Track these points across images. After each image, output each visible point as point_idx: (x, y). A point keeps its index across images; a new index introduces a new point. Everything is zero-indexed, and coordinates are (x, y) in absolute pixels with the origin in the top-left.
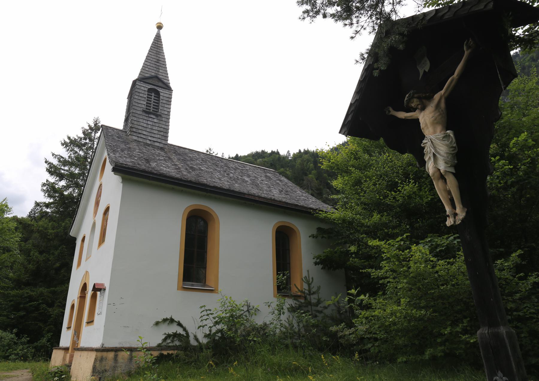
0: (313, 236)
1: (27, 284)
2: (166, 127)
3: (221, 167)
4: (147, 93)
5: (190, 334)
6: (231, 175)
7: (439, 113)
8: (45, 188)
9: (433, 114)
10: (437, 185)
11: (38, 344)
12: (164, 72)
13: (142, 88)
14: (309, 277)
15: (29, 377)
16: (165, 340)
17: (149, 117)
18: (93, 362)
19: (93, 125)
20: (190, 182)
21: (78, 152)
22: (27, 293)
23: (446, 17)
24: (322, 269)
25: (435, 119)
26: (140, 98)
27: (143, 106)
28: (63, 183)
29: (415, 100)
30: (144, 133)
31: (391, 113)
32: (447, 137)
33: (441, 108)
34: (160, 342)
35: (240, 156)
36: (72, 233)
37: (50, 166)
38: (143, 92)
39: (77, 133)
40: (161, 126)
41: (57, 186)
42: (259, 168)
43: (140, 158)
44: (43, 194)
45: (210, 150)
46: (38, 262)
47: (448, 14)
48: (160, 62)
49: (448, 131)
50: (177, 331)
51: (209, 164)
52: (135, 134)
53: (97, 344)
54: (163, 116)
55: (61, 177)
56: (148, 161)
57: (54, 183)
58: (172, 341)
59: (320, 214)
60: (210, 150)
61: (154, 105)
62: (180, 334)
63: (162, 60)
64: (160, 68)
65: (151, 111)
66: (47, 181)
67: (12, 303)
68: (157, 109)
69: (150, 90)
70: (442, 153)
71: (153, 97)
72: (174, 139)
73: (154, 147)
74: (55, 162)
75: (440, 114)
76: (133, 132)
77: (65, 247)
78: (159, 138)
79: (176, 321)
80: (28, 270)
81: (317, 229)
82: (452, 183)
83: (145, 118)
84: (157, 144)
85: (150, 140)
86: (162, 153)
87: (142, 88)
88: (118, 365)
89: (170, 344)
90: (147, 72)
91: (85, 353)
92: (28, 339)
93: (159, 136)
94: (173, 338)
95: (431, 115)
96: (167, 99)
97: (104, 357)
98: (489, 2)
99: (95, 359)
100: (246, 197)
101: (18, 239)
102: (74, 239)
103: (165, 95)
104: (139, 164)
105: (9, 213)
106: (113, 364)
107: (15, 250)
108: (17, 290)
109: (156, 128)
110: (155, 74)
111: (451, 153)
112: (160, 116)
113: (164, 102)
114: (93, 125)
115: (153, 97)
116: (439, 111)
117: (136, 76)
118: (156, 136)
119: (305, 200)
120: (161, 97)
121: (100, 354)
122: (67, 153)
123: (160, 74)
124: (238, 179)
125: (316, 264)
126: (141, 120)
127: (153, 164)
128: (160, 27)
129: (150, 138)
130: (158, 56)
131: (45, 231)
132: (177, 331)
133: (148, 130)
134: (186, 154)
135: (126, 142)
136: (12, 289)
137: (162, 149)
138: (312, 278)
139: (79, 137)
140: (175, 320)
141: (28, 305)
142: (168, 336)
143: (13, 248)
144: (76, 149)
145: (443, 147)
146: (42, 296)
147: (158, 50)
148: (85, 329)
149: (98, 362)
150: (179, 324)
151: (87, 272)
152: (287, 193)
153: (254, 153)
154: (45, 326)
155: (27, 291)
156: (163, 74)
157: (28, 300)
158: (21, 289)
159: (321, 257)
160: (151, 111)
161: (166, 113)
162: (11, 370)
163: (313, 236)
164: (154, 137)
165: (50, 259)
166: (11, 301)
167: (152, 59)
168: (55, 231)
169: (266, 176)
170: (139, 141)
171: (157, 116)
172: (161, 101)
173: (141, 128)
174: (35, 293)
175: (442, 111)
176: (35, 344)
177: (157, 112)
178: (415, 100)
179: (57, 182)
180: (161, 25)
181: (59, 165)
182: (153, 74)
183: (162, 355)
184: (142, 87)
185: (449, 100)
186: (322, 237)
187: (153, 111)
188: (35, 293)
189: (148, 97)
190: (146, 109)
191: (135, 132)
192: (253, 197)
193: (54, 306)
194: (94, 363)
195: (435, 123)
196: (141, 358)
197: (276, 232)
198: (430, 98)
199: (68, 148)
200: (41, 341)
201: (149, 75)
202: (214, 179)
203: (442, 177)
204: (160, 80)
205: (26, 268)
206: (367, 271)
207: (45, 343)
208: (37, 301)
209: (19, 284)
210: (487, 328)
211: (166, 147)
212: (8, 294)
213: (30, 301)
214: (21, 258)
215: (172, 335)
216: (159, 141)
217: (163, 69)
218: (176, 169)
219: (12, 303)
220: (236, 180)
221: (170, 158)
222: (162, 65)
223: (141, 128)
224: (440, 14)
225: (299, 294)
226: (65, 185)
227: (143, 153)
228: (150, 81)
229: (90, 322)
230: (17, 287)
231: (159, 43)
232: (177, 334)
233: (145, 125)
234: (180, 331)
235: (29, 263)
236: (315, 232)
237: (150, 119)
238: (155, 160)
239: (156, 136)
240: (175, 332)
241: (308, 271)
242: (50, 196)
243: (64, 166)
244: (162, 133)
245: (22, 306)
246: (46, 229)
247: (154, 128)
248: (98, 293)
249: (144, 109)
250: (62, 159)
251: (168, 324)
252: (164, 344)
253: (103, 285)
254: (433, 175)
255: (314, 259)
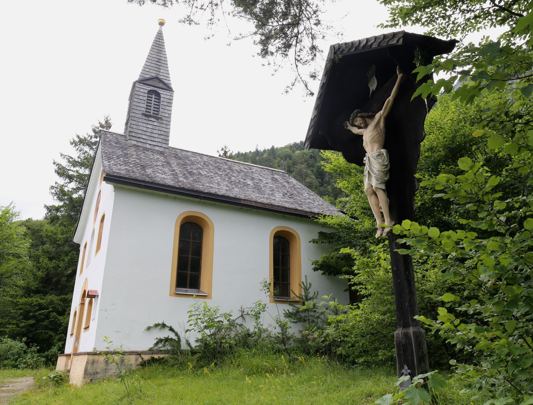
0: (314, 241)
1: (37, 292)
2: (166, 130)
3: (224, 171)
4: (146, 95)
5: (181, 339)
6: (233, 178)
7: (376, 132)
8: (53, 191)
9: (372, 132)
10: (371, 201)
11: (49, 353)
12: (166, 72)
13: (142, 90)
14: (306, 282)
15: (32, 382)
16: (157, 344)
17: (149, 120)
18: (85, 365)
19: (103, 123)
20: (183, 189)
21: (88, 151)
22: (36, 301)
23: (373, 46)
24: (322, 274)
25: (373, 138)
26: (139, 101)
27: (143, 109)
28: (73, 185)
29: (358, 119)
30: (144, 137)
31: (348, 128)
32: (380, 155)
33: (379, 127)
34: (152, 346)
35: (277, 148)
36: (76, 240)
37: (58, 167)
38: (142, 94)
39: (86, 132)
40: (161, 129)
41: (66, 189)
42: (267, 169)
43: (135, 165)
44: (51, 196)
45: (226, 147)
46: (48, 269)
47: (375, 44)
48: (162, 61)
49: (382, 150)
50: (168, 336)
51: (211, 167)
52: (134, 139)
53: (90, 350)
54: (163, 118)
55: (71, 178)
56: (143, 167)
57: (63, 185)
58: (164, 346)
59: (320, 219)
60: (226, 147)
61: (154, 107)
62: (172, 339)
63: (163, 59)
64: (161, 68)
65: (151, 113)
66: (56, 183)
67: (21, 311)
68: (157, 111)
69: (150, 92)
70: (375, 170)
71: (153, 99)
72: (172, 143)
73: (153, 151)
74: (64, 163)
75: (378, 133)
76: (133, 136)
77: (75, 253)
78: (159, 142)
79: (168, 327)
80: (38, 277)
81: (319, 233)
82: (382, 196)
83: (145, 122)
84: (157, 148)
85: (150, 144)
86: (162, 158)
87: (142, 90)
88: (109, 368)
89: (162, 349)
90: (147, 73)
91: (80, 357)
92: (38, 348)
93: (159, 140)
94: (165, 343)
95: (370, 134)
96: (168, 101)
97: (95, 360)
98: (400, 38)
99: (87, 362)
100: (242, 202)
101: (28, 245)
102: (78, 246)
103: (166, 97)
104: (133, 172)
105: (17, 217)
106: (105, 367)
107: (25, 256)
108: (26, 298)
109: (157, 132)
110: (156, 75)
111: (382, 171)
112: (161, 118)
113: (165, 104)
114: (103, 123)
115: (153, 99)
116: (377, 131)
117: (137, 78)
118: (156, 140)
119: (310, 203)
120: (162, 99)
121: (91, 357)
122: (76, 152)
123: (161, 74)
124: (239, 182)
125: (315, 269)
126: (141, 124)
127: (149, 171)
128: (162, 24)
129: (150, 142)
130: (160, 55)
131: (55, 237)
132: (168, 336)
133: (148, 134)
134: (187, 158)
135: (123, 148)
136: (22, 296)
137: (162, 153)
138: (310, 284)
139: (90, 136)
140: (167, 325)
141: (37, 313)
142: (160, 341)
143: (23, 254)
144: (86, 148)
145: (376, 165)
146: (52, 304)
147: (160, 49)
148: (83, 334)
149: (90, 365)
150: (171, 329)
151: (86, 279)
152: (291, 196)
153: (291, 144)
154: (56, 335)
155: (36, 299)
156: (165, 75)
157: (37, 308)
158: (30, 297)
159: (318, 262)
160: (151, 113)
161: (167, 115)
162: (18, 377)
163: (314, 241)
164: (154, 141)
165: (60, 265)
166: (21, 309)
167: (152, 59)
168: (64, 236)
169: (273, 179)
170: (138, 146)
171: (157, 119)
172: (162, 103)
173: (140, 132)
174: (45, 301)
175: (380, 130)
176: (46, 353)
177: (157, 114)
178: (358, 119)
179: (66, 185)
180: (163, 21)
181: (69, 166)
182: (154, 75)
183: (153, 359)
184: (142, 89)
185: (389, 120)
186: (322, 242)
187: (153, 113)
188: (45, 301)
189: (147, 99)
190: (146, 111)
191: (134, 136)
192: (249, 202)
193: (65, 314)
194: (86, 365)
195: (373, 141)
196: (132, 360)
197: (274, 237)
198: (372, 117)
199: (77, 147)
200: (51, 350)
201: (149, 76)
202: (213, 184)
203: (375, 193)
204: (160, 81)
205: (36, 275)
206: (344, 277)
207: (55, 352)
208: (47, 309)
209: (28, 292)
210: (402, 328)
211: (167, 150)
212: (17, 302)
213: (40, 310)
214: (30, 264)
215: (163, 340)
216: (159, 144)
217: (164, 68)
218: (173, 175)
219: (21, 311)
220: (236, 184)
221: (168, 163)
222: (163, 65)
223: (140, 132)
224: (370, 43)
225: (298, 299)
226: (75, 187)
227: (140, 159)
228: (150, 82)
229: (87, 328)
230: (26, 295)
231: (161, 41)
232: (169, 339)
233: (145, 129)
234: (172, 336)
235: (39, 269)
236: (316, 237)
237: (150, 123)
238: (151, 167)
239: (156, 140)
240: (166, 336)
241: (306, 276)
242: (60, 199)
243: (74, 167)
244: (162, 137)
245: (31, 314)
246: (55, 234)
247: (154, 131)
248: (93, 299)
249: (143, 112)
250: (71, 160)
251: (160, 329)
252: (156, 348)
253: (96, 291)
254: (367, 190)
255: (312, 264)
